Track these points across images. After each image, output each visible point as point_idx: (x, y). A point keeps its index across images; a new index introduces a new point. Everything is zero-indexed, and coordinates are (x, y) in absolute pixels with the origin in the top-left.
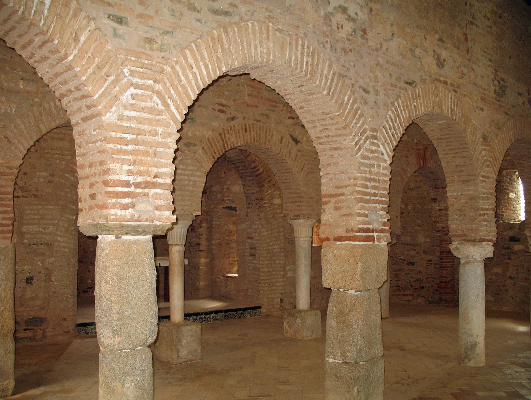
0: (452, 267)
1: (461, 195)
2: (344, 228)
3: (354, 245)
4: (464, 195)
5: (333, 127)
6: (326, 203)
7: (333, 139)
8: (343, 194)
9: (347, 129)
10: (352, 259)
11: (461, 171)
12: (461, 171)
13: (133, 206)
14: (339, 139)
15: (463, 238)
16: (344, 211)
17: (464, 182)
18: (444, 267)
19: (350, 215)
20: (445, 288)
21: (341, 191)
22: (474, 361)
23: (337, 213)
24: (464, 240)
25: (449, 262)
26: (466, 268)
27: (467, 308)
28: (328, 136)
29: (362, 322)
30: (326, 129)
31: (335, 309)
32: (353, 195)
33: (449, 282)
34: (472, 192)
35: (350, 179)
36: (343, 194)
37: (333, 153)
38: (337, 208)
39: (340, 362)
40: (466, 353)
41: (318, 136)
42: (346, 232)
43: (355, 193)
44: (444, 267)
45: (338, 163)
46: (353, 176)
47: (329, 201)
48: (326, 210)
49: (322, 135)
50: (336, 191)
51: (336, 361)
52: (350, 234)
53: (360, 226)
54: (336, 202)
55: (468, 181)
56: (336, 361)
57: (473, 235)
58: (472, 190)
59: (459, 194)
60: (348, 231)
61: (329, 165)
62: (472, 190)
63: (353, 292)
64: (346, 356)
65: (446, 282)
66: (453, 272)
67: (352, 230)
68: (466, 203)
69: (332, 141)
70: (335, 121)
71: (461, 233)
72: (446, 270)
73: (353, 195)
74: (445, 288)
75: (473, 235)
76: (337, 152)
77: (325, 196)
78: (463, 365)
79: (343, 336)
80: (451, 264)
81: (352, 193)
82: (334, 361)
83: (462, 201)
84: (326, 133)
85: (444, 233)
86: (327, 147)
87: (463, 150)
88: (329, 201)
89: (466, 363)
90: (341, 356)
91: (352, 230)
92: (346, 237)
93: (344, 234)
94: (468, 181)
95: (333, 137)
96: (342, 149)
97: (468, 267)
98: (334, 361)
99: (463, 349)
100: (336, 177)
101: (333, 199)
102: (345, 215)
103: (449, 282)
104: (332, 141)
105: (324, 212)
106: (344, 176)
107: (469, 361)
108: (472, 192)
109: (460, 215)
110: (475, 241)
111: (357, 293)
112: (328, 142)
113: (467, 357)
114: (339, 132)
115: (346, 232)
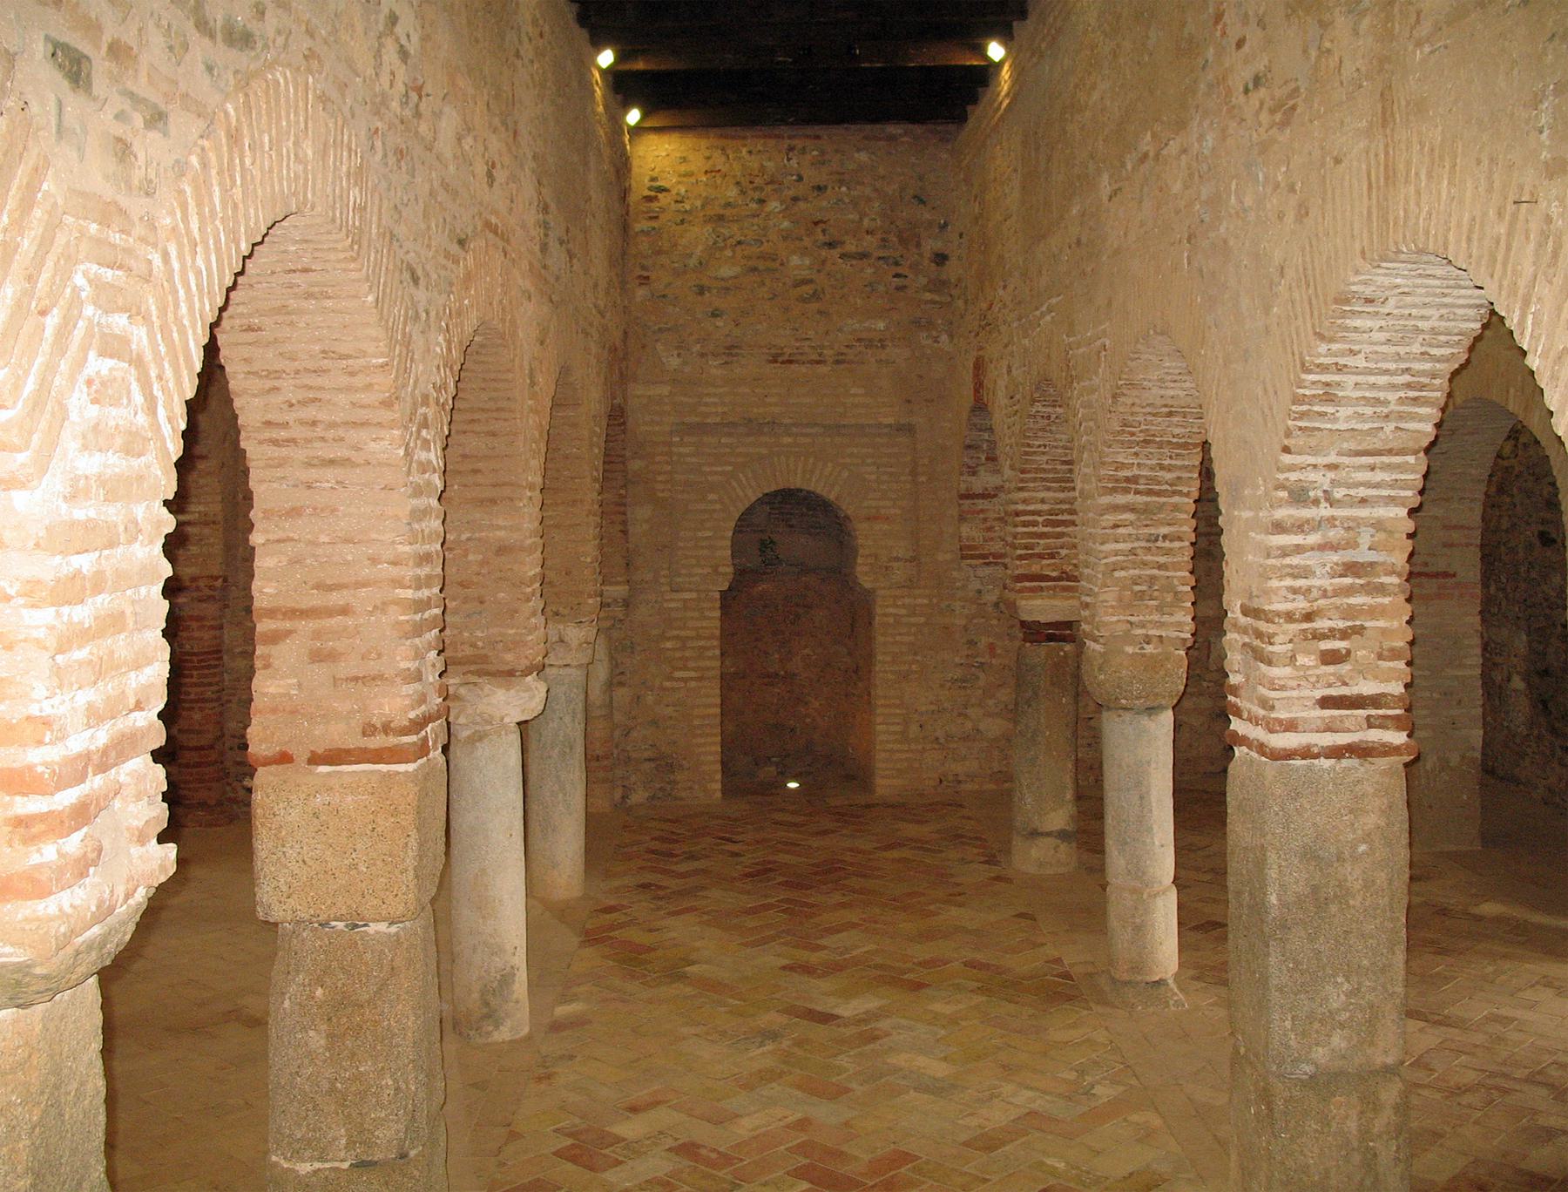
0: (219, 699)
1: (468, 539)
2: (353, 723)
3: (389, 775)
4: (480, 540)
5: (342, 399)
6: (275, 638)
7: (331, 434)
8: (345, 611)
9: (396, 407)
10: (384, 823)
11: (476, 471)
12: (476, 471)
13: (910, 1029)
14: (354, 435)
15: (473, 668)
16: (345, 668)
17: (480, 502)
18: (197, 701)
19: (380, 677)
20: (198, 765)
21: (336, 599)
22: (509, 1023)
23: (321, 672)
24: (480, 673)
25: (210, 684)
26: (479, 752)
27: (483, 870)
28: (314, 423)
29: (417, 1017)
30: (314, 400)
31: (319, 992)
32: (384, 612)
33: (212, 747)
34: (502, 534)
35: (374, 561)
36: (345, 611)
37: (313, 473)
38: (317, 657)
39: (346, 1165)
40: (487, 1004)
41: (269, 417)
42: (364, 734)
43: (393, 609)
44: (197, 701)
45: (334, 510)
46: (388, 554)
47: (288, 633)
48: (276, 663)
49: (290, 417)
50: (315, 600)
51: (327, 1165)
52: (378, 741)
53: (412, 715)
54: (317, 635)
55: (493, 501)
56: (327, 1165)
57: (509, 657)
58: (505, 528)
59: (464, 537)
60: (369, 730)
61: (295, 512)
62: (505, 528)
63: (382, 927)
64: (369, 1145)
65: (202, 748)
66: (221, 714)
67: (386, 729)
68: (483, 563)
69: (323, 439)
70: (359, 381)
71: (468, 651)
72: (201, 709)
73: (384, 612)
74: (198, 765)
75: (509, 657)
76: (330, 474)
77: (271, 613)
78: (480, 1041)
79: (357, 1078)
80: (215, 688)
81: (382, 608)
82: (317, 1165)
83: (471, 557)
84: (310, 412)
85: (195, 594)
86: (299, 454)
87: (495, 415)
88: (288, 633)
89: (489, 1033)
90: (350, 1145)
91: (386, 729)
92: (365, 750)
93: (355, 741)
94: (493, 501)
95: (332, 425)
96: (354, 465)
97: (483, 750)
98: (317, 1165)
99: (476, 995)
100: (320, 551)
101: (305, 626)
102: (356, 679)
103: (212, 747)
104: (323, 439)
105: (267, 666)
106: (349, 552)
107: (497, 1028)
108: (502, 534)
109: (466, 600)
110: (511, 673)
111: (394, 929)
112: (308, 441)
113: (491, 1015)
114: (363, 414)
115: (364, 734)
